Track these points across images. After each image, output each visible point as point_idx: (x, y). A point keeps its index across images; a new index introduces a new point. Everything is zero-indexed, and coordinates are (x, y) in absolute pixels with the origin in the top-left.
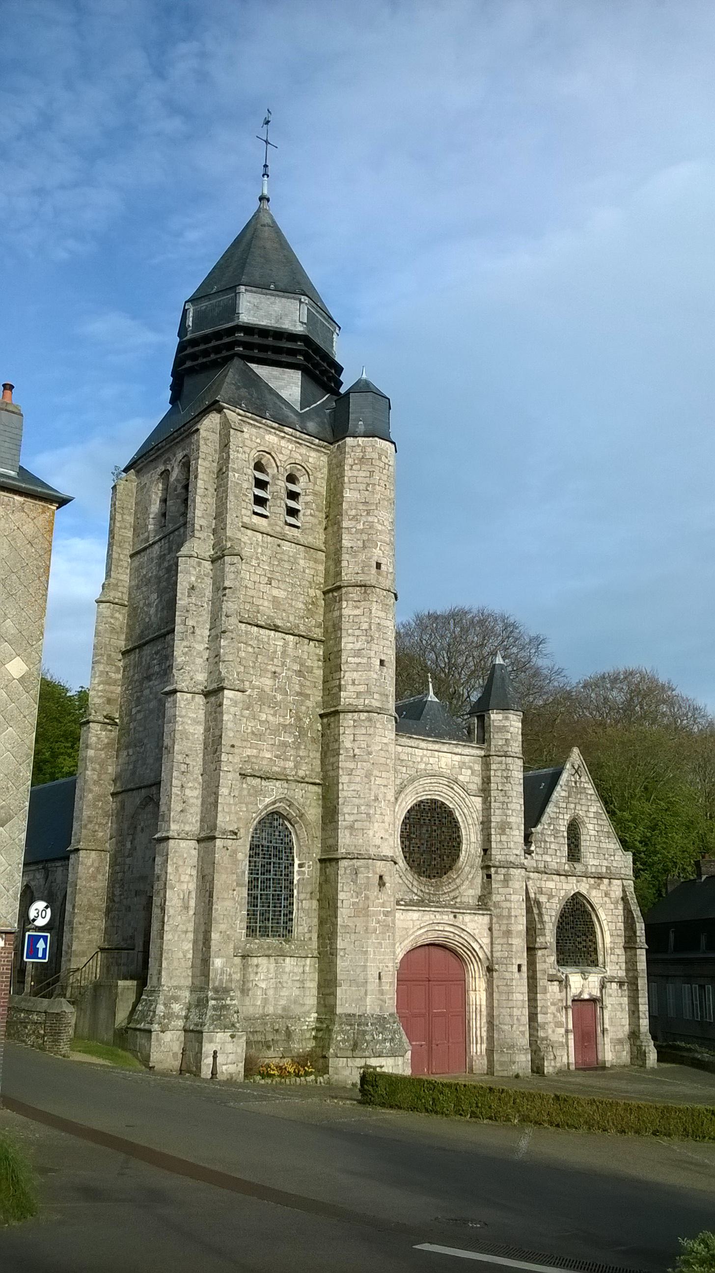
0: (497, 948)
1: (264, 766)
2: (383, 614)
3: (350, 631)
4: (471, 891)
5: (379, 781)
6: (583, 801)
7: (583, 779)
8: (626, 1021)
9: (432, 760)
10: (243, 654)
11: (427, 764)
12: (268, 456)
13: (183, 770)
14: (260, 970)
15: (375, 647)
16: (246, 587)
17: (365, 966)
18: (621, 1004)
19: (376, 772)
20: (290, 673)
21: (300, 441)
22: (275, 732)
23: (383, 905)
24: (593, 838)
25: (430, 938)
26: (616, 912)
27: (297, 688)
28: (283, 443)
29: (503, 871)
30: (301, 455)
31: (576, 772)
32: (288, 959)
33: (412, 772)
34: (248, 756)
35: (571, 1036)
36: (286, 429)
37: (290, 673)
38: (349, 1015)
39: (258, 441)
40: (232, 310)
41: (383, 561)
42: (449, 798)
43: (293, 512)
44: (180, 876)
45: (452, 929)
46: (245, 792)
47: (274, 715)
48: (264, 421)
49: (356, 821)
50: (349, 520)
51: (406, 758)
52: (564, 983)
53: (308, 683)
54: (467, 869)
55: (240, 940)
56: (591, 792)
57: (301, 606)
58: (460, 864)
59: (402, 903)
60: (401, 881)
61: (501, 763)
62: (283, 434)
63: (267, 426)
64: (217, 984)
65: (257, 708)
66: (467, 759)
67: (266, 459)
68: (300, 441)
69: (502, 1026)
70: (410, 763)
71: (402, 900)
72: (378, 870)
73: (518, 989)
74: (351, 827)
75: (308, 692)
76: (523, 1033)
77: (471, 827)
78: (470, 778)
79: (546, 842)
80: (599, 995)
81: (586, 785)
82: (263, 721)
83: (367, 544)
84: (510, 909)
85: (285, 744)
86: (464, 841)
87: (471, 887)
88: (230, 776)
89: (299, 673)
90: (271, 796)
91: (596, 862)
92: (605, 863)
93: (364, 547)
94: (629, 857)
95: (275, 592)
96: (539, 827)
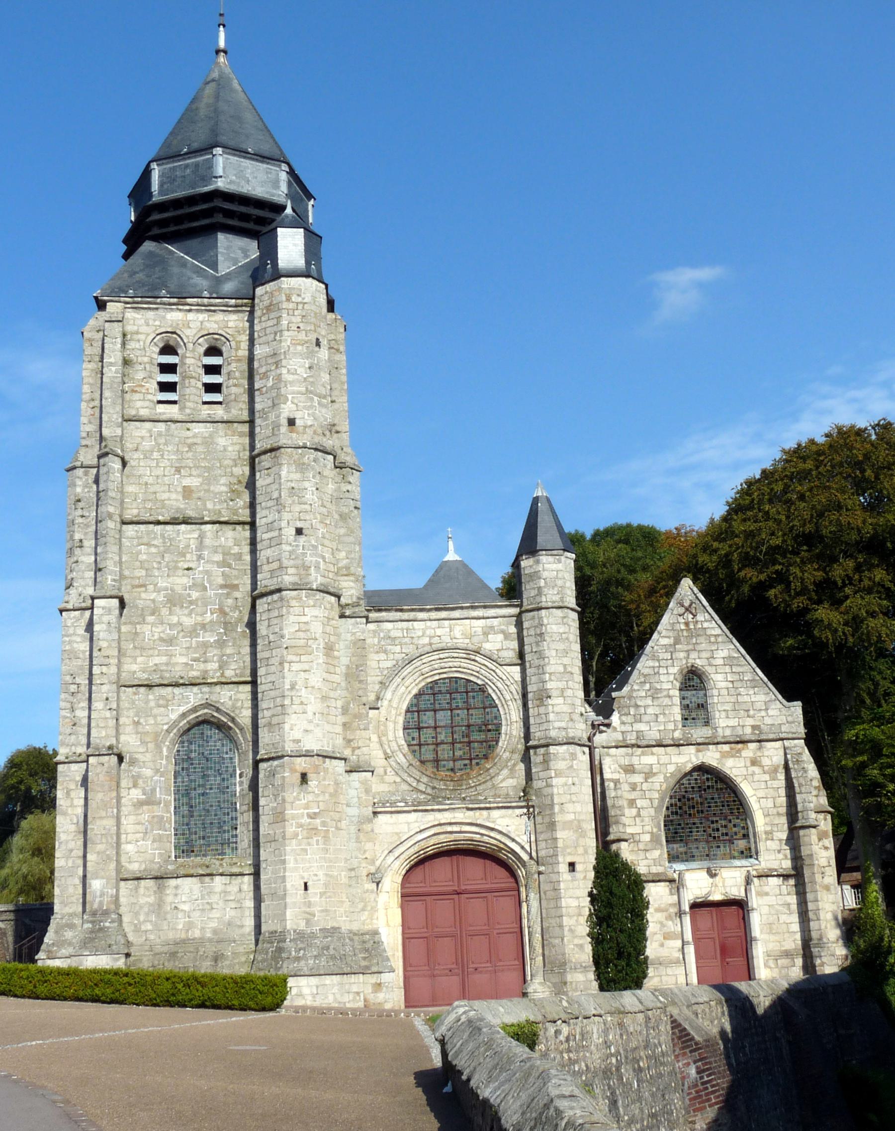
0: (542, 845)
1: (177, 672)
2: (297, 476)
3: (263, 504)
4: (511, 781)
5: (295, 667)
6: (703, 646)
7: (700, 617)
8: (796, 927)
9: (439, 632)
10: (144, 557)
11: (431, 637)
12: (175, 336)
13: (72, 690)
14: (180, 891)
15: (286, 516)
16: (146, 484)
17: (284, 877)
18: (789, 904)
19: (290, 658)
20: (208, 567)
21: (213, 308)
22: (192, 632)
23: (307, 807)
24: (725, 692)
25: (432, 844)
26: (776, 784)
27: (220, 581)
28: (191, 316)
29: (542, 751)
30: (215, 322)
31: (687, 609)
32: (218, 878)
33: (411, 650)
34: (156, 665)
35: (691, 950)
36: (189, 300)
37: (208, 567)
38: (272, 933)
39: (157, 323)
40: (208, 174)
41: (298, 415)
42: (474, 671)
43: (212, 388)
44: (72, 799)
45: (474, 829)
46: (152, 704)
47: (190, 614)
48: (159, 300)
49: (273, 715)
50: (261, 379)
51: (400, 634)
52: (676, 884)
53: (235, 573)
54: (507, 755)
55: (152, 862)
56: (718, 631)
57: (224, 489)
58: (498, 750)
59: (388, 805)
60: (398, 780)
61: (533, 618)
62: (188, 307)
63: (164, 304)
64: (96, 906)
65: (165, 611)
66: (495, 622)
67: (173, 340)
68: (213, 308)
69: (552, 940)
70: (407, 640)
71: (388, 802)
72: (297, 767)
73: (570, 893)
74: (270, 724)
75: (236, 582)
76: (581, 947)
77: (510, 703)
78: (500, 643)
79: (637, 706)
80: (743, 894)
81: (706, 625)
82: (175, 625)
83: (276, 402)
84: (552, 795)
85: (205, 645)
86: (504, 723)
87: (512, 775)
88: (105, 688)
89: (224, 564)
90: (187, 703)
91: (733, 722)
92: (750, 722)
93: (274, 405)
94: (797, 708)
95: (187, 482)
96: (626, 689)
